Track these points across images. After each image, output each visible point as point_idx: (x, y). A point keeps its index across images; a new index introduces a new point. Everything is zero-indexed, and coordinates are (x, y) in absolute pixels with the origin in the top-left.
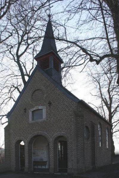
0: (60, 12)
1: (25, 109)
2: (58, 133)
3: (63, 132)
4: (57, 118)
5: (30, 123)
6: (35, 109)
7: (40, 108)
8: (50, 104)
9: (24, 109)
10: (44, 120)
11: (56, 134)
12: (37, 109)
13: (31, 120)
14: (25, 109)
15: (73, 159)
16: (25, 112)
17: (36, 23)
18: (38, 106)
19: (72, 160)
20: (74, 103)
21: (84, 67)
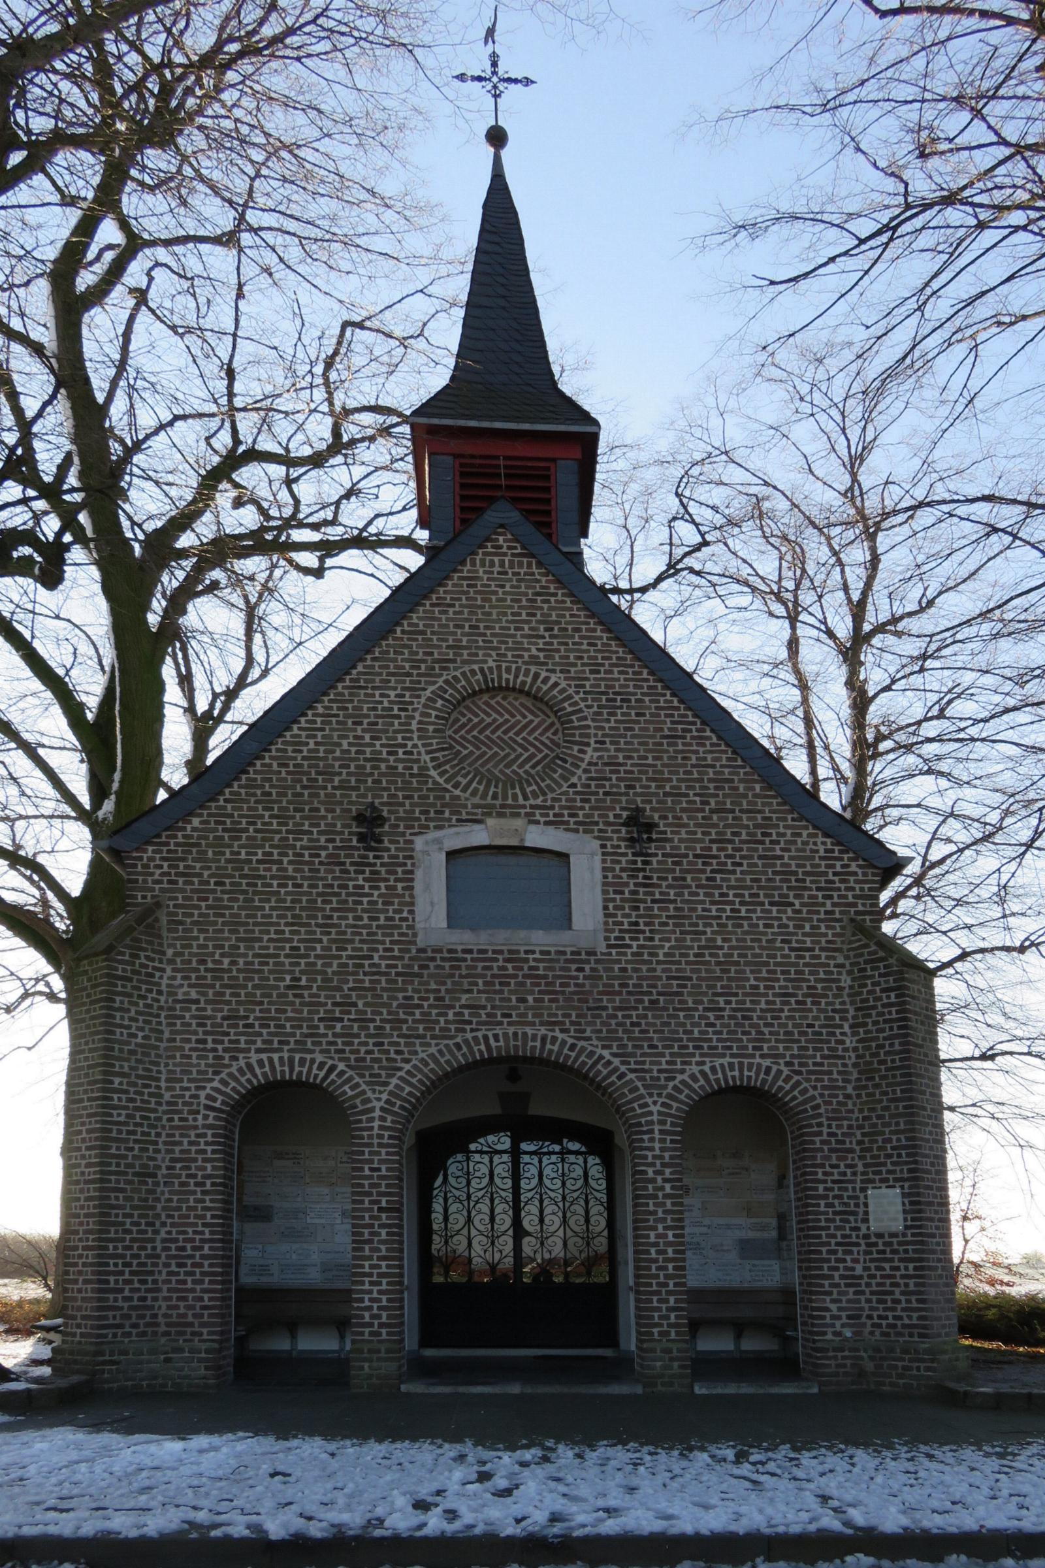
0: (285, 395)
1: (370, 824)
2: (726, 1061)
3: (767, 1062)
4: (711, 945)
5: (421, 943)
6: (478, 836)
7: (538, 837)
8: (639, 828)
9: (360, 818)
10: (584, 944)
11: (705, 1070)
12: (514, 842)
13: (440, 919)
14: (370, 824)
15: (859, 1270)
16: (362, 838)
17: (218, 250)
18: (519, 823)
19: (852, 1280)
20: (854, 867)
21: (983, 293)
